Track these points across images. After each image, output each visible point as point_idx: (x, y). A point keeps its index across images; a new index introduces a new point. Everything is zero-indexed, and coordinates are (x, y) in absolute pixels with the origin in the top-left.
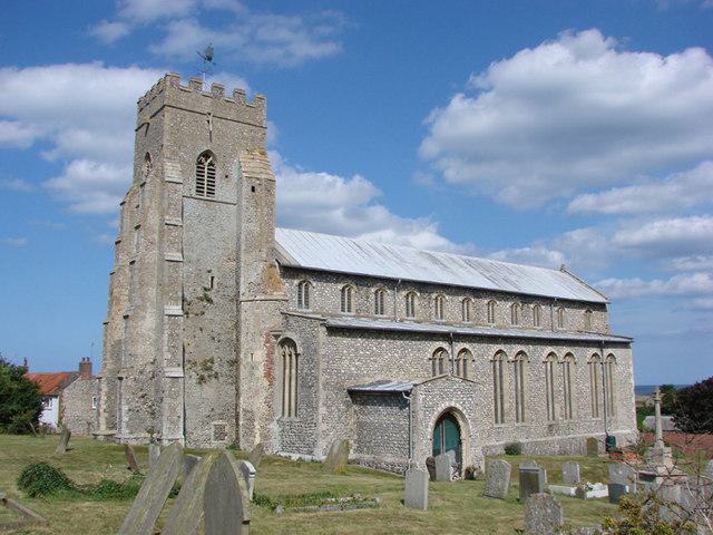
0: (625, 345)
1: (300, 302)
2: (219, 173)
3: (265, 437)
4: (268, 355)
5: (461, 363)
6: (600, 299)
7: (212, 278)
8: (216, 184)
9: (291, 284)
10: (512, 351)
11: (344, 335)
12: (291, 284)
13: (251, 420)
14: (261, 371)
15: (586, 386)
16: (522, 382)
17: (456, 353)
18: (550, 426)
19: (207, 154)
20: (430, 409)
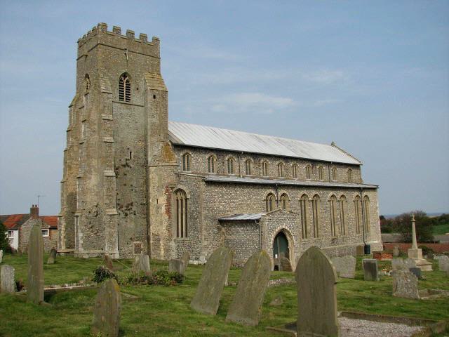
2: (133, 87)
3: (167, 250)
6: (357, 163)
17: (279, 196)
19: (125, 75)
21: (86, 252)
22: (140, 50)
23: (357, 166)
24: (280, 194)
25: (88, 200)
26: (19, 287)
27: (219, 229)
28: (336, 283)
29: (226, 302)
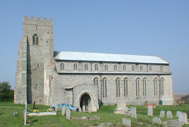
0: (169, 74)
1: (124, 70)
2: (39, 39)
3: (49, 101)
4: (49, 81)
5: (155, 81)
6: (168, 63)
7: (38, 64)
8: (39, 42)
9: (58, 64)
10: (122, 78)
11: (135, 75)
12: (58, 64)
13: (46, 97)
14: (48, 85)
15: (152, 87)
16: (146, 88)
17: (102, 79)
18: (137, 98)
19: (36, 35)
20: (79, 93)
21: (17, 101)
22: (43, 24)
23: (168, 65)
24: (160, 78)
25: (18, 83)
26: (17, 114)
27: (65, 93)
28: (65, 115)
29: (117, 122)
